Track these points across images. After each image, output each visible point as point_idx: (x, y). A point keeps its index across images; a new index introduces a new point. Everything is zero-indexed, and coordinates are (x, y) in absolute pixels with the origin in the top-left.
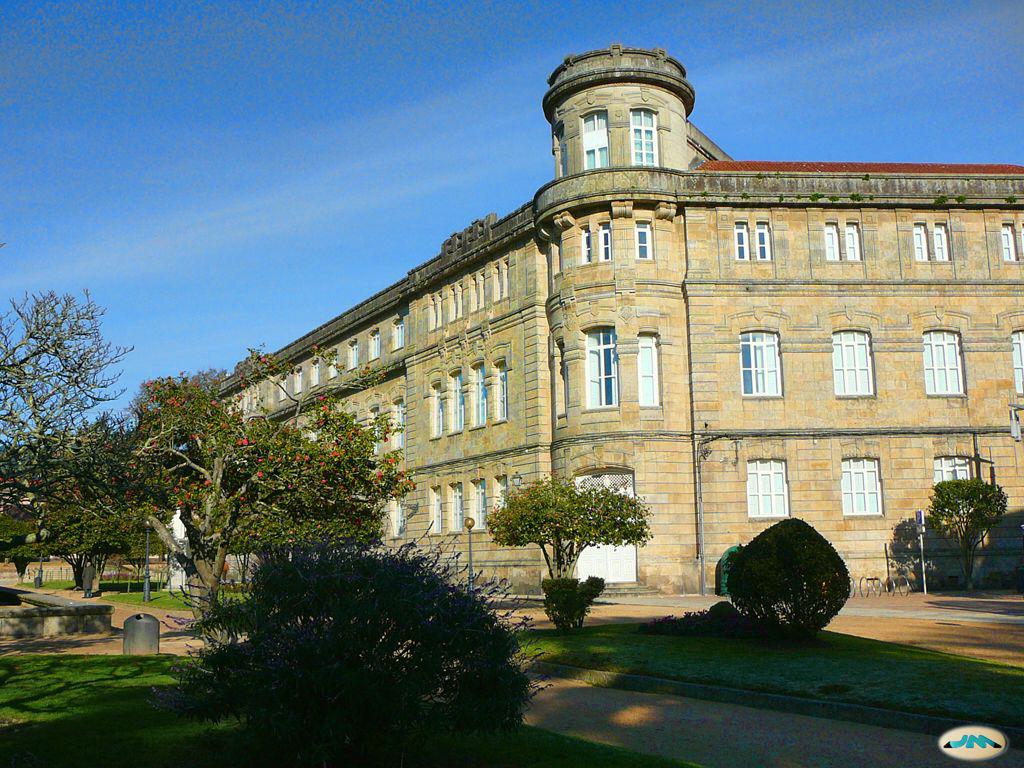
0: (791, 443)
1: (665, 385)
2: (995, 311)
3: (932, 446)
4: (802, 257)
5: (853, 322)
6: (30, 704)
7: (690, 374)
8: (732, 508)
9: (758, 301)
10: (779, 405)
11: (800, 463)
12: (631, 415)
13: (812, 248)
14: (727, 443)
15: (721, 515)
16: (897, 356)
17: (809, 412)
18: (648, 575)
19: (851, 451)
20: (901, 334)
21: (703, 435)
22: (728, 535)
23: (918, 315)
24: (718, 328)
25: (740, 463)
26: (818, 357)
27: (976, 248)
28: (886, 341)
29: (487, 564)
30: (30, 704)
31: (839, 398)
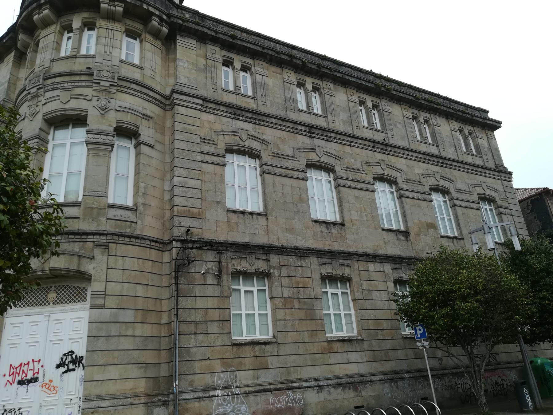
0: (274, 259)
1: (142, 185)
2: (417, 171)
3: (391, 271)
4: (280, 101)
5: (322, 159)
6: (19, 367)
7: (201, 162)
8: (214, 328)
9: (241, 124)
10: (262, 220)
11: (283, 279)
12: (95, 211)
13: (287, 95)
14: (210, 256)
15: (200, 337)
16: (357, 192)
17: (290, 230)
18: (449, 396)
19: (328, 270)
20: (358, 177)
21: (182, 241)
22: (208, 362)
23: (368, 164)
24: (204, 140)
25: (225, 278)
26: (295, 182)
27: (399, 126)
28: (347, 179)
29: (374, 378)
30: (19, 367)
31: (315, 221)
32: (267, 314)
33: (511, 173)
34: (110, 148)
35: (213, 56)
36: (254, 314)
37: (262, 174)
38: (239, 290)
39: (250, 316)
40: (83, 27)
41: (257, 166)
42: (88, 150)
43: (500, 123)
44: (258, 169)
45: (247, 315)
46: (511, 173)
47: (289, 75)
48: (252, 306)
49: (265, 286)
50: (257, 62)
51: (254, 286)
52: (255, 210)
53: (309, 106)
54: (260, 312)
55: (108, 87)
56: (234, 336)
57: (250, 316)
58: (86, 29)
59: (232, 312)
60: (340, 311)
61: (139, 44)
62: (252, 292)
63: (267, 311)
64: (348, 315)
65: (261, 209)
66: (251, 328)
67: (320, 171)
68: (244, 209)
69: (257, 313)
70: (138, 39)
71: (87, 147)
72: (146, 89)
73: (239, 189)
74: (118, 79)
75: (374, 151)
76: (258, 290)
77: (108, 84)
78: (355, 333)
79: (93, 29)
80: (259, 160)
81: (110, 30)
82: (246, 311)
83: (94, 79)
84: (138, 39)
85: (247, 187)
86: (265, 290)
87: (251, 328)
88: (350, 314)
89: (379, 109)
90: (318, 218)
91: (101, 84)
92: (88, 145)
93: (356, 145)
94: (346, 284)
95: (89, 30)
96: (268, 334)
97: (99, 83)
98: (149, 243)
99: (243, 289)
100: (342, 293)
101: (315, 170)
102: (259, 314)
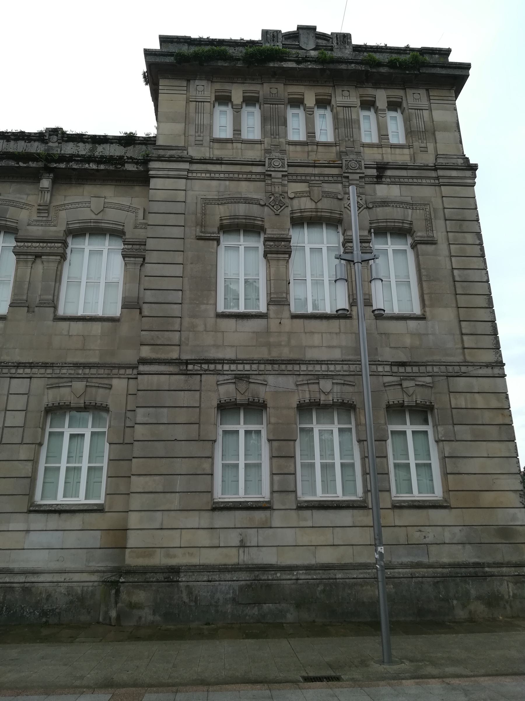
33: (474, 168)
34: (287, 256)
39: (328, 468)
42: (126, 264)
45: (324, 466)
46: (474, 168)
47: (200, 88)
49: (350, 423)
50: (410, 92)
51: (333, 423)
52: (406, 311)
53: (311, 133)
54: (70, 465)
55: (357, 180)
57: (328, 468)
61: (375, 114)
63: (353, 459)
65: (417, 311)
68: (89, 313)
69: (412, 462)
70: (399, 111)
71: (124, 260)
72: (304, 168)
74: (288, 166)
75: (440, 185)
77: (279, 175)
82: (341, 459)
84: (399, 111)
85: (307, 279)
86: (350, 430)
88: (352, 465)
89: (402, 108)
91: (350, 178)
92: (126, 259)
93: (199, 175)
94: (350, 417)
98: (387, 368)
100: (341, 430)
101: (225, 235)
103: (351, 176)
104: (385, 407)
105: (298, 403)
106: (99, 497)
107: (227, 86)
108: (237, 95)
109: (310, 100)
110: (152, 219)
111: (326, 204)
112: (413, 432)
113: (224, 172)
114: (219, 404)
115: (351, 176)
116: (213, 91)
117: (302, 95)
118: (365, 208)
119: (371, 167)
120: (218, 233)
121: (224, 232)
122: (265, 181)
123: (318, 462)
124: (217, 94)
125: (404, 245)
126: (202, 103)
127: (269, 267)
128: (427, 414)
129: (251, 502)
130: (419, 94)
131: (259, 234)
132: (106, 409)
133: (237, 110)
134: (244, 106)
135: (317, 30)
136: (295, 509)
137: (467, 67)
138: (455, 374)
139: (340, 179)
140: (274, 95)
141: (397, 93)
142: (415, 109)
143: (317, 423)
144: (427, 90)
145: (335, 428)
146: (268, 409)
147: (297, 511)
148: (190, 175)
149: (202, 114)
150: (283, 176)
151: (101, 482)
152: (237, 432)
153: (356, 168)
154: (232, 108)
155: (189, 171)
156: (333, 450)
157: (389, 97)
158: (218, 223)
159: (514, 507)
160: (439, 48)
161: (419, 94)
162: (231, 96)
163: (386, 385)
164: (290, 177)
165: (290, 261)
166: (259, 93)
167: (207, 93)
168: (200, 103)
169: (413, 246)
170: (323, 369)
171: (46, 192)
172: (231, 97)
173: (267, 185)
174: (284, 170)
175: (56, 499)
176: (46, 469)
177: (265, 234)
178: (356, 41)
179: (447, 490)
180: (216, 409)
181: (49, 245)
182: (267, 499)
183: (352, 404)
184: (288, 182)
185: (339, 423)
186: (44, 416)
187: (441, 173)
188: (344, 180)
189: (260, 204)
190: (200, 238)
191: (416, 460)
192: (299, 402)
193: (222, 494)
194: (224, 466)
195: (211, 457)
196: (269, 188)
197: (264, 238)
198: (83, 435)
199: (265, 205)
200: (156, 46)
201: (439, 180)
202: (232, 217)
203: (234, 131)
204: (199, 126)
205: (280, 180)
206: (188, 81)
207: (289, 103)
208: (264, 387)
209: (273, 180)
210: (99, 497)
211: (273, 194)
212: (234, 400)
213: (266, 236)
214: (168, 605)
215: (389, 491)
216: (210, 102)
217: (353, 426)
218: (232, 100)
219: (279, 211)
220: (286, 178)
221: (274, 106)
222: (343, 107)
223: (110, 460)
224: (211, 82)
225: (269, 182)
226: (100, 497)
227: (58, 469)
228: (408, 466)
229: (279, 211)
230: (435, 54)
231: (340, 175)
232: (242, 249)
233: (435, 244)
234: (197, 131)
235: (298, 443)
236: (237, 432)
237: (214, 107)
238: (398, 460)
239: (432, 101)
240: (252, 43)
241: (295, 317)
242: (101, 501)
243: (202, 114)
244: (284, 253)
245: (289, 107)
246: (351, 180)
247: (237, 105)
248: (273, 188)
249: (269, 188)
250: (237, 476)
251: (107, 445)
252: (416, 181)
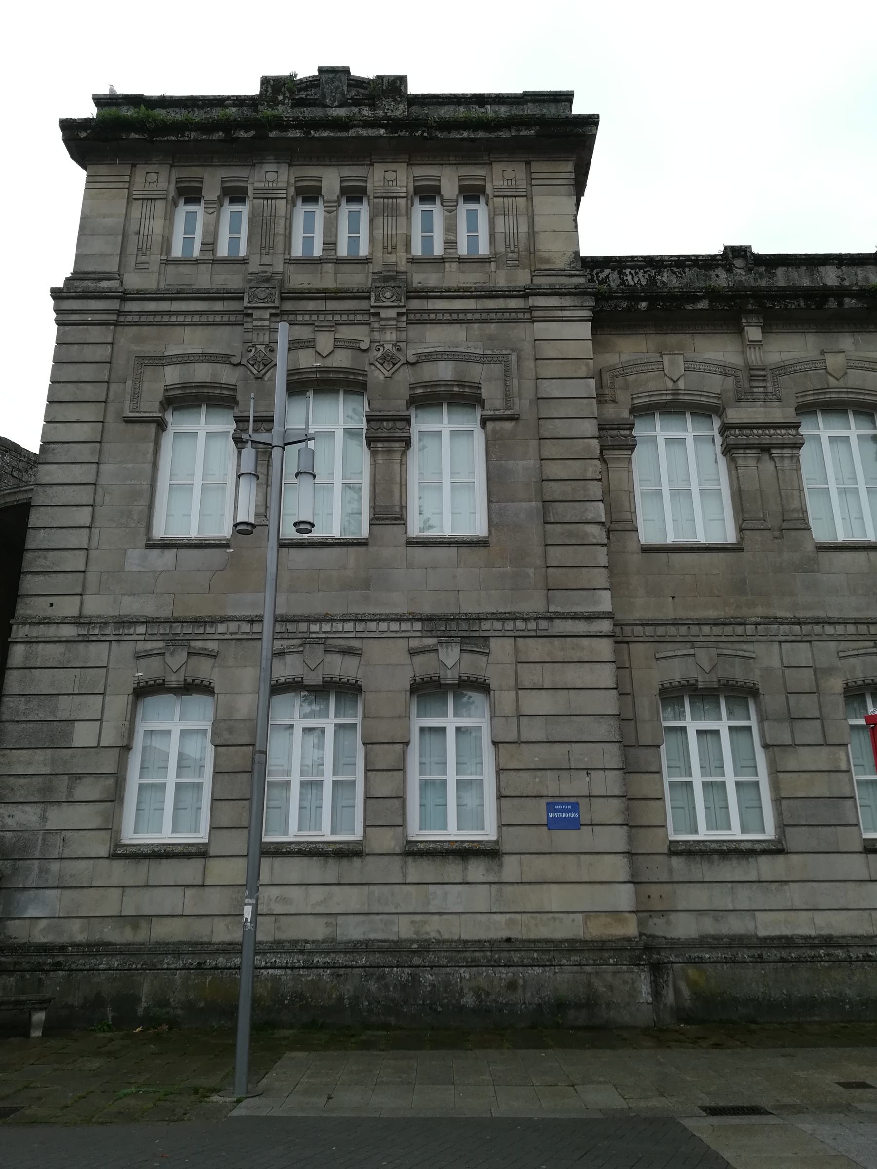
32: (757, 784)
35: (151, 188)
36: (444, 783)
37: (727, 450)
38: (684, 729)
39: (714, 788)
40: (295, 196)
41: (716, 432)
43: (598, 116)
44: (718, 440)
48: (718, 764)
49: (749, 719)
56: (867, 830)
57: (714, 788)
58: (182, 202)
59: (855, 778)
60: (445, 773)
62: (716, 733)
64: (746, 788)
66: (719, 819)
67: (471, 410)
69: (730, 779)
72: (348, 301)
73: (839, 493)
76: (338, 727)
78: (770, 833)
79: (359, 200)
80: (720, 417)
81: (153, 202)
82: (736, 775)
83: (372, 307)
85: (829, 486)
86: (749, 729)
87: (719, 819)
90: (669, 542)
91: (383, 315)
94: (719, 707)
95: (188, 201)
96: (763, 831)
97: (378, 314)
99: (693, 726)
102: (738, 784)
103: (384, 313)
104: (658, 692)
105: (661, 687)
106: (676, 831)
107: (313, 171)
108: (450, 187)
109: (450, 187)
110: (99, 392)
111: (342, 359)
112: (699, 732)
113: (222, 313)
114: (275, 685)
115: (384, 313)
116: (173, 180)
117: (318, 180)
118: (404, 364)
119: (289, 296)
120: (408, 409)
121: (417, 408)
122: (370, 324)
123: (697, 779)
124: (299, 184)
125: (226, 424)
126: (514, 199)
127: (374, 464)
128: (866, 702)
129: (748, 841)
130: (514, 171)
131: (474, 407)
132: (752, 692)
133: (332, 209)
134: (344, 202)
135: (352, 74)
136: (861, 853)
137: (592, 121)
138: (715, 637)
139: (366, 317)
140: (390, 183)
141: (235, 173)
142: (504, 197)
143: (693, 719)
144: (528, 163)
145: (329, 724)
146: (492, 692)
147: (864, 856)
148: (122, 319)
149: (151, 220)
150: (398, 314)
151: (354, 806)
152: (443, 730)
153: (392, 299)
154: (442, 204)
155: (119, 313)
156: (721, 760)
157: (318, 180)
158: (406, 393)
159: (613, 856)
160: (203, 97)
161: (514, 171)
162: (440, 186)
163: (841, 654)
164: (411, 316)
165: (408, 452)
166: (366, 181)
167: (163, 184)
168: (510, 199)
169: (484, 422)
170: (231, 630)
171: (752, 349)
172: (439, 187)
173: (247, 331)
174: (401, 304)
175: (286, 832)
176: (141, 787)
177: (483, 408)
178: (414, 88)
179: (782, 826)
180: (408, 693)
181: (755, 431)
182: (493, 837)
183: (751, 688)
184: (407, 324)
185: (456, 715)
186: (132, 702)
187: (533, 301)
188: (372, 319)
189: (231, 364)
190: (129, 421)
191: (736, 775)
192: (138, 683)
193: (421, 829)
194: (425, 784)
195: (402, 769)
196: (248, 336)
197: (482, 415)
198: (168, 732)
199: (239, 364)
200: (90, 111)
201: (531, 313)
202: (184, 386)
203: (324, 244)
204: (145, 237)
205: (393, 322)
206: (134, 165)
207: (415, 193)
208: (484, 658)
209: (255, 323)
210: (352, 831)
211: (382, 345)
212: (300, 679)
213: (485, 412)
214: (421, 1002)
215: (664, 826)
216: (525, 196)
217: (753, 723)
218: (442, 193)
219: (263, 372)
220: (404, 318)
221: (390, 200)
222: (143, 199)
223: (217, 773)
224: (290, 165)
225: (250, 326)
226: (354, 830)
227: (164, 786)
228: (689, 785)
229: (263, 372)
230: (526, 102)
231: (239, 312)
232: (202, 436)
233: (517, 419)
234: (508, 244)
235: (663, 748)
236: (443, 730)
237: (412, 205)
238: (741, 776)
239: (534, 182)
240: (240, 101)
241: (412, 543)
242: (357, 835)
243: (151, 220)
244: (400, 440)
245: (416, 201)
246: (256, 320)
247: (451, 200)
248: (255, 336)
249: (248, 336)
250: (199, 799)
251: (359, 744)
252: (522, 317)
